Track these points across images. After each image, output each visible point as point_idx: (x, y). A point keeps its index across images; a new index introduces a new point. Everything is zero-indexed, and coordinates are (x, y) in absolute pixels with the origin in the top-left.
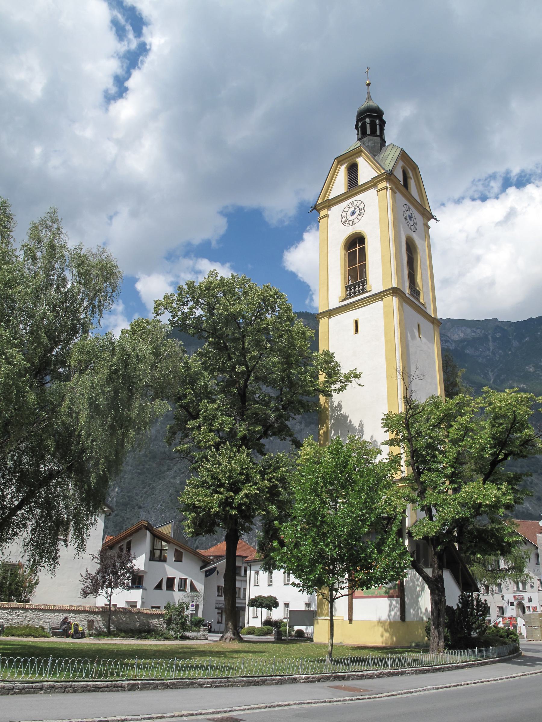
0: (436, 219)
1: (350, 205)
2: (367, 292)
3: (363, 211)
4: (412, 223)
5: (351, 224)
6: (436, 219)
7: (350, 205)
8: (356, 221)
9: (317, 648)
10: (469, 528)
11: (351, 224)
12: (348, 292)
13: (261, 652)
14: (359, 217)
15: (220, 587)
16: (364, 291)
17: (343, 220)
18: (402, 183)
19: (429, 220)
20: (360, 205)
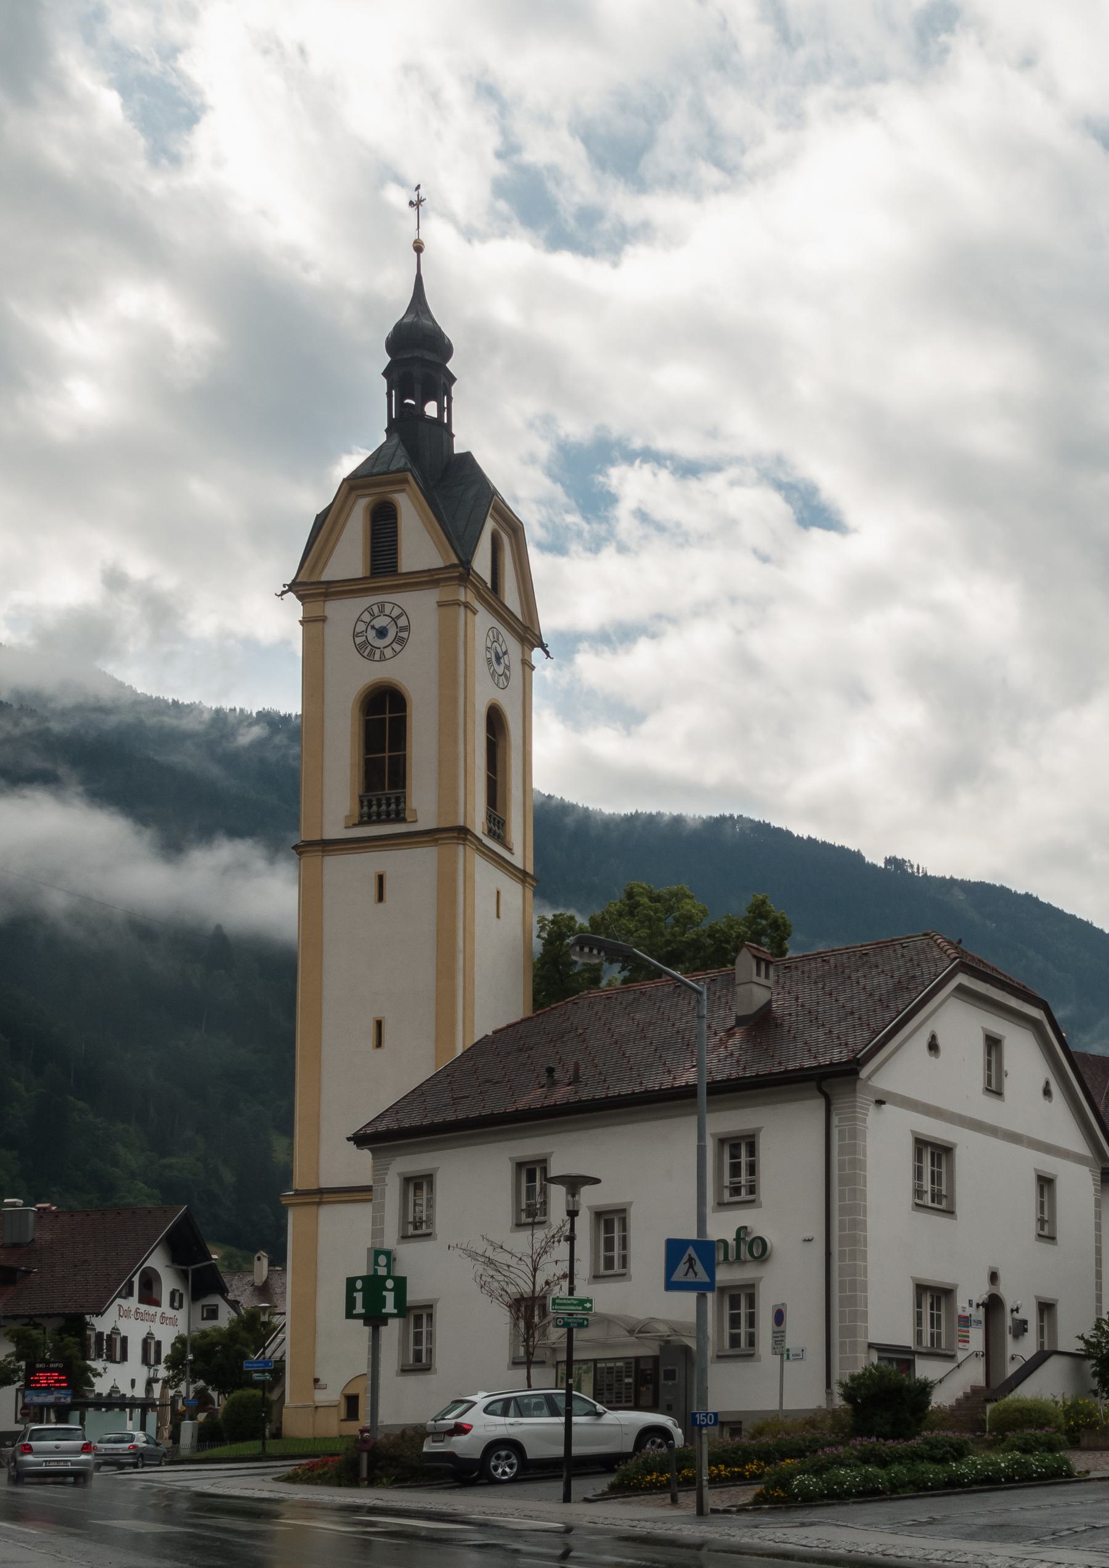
0: (547, 653)
1: (376, 609)
2: (403, 820)
3: (404, 635)
4: (500, 669)
5: (377, 657)
6: (547, 653)
7: (376, 609)
8: (388, 652)
9: (320, 1476)
10: (205, 1414)
11: (377, 657)
12: (365, 809)
13: (13, 1562)
14: (397, 647)
15: (588, 1305)
16: (400, 818)
17: (359, 640)
18: (489, 585)
19: (533, 646)
20: (398, 617)
